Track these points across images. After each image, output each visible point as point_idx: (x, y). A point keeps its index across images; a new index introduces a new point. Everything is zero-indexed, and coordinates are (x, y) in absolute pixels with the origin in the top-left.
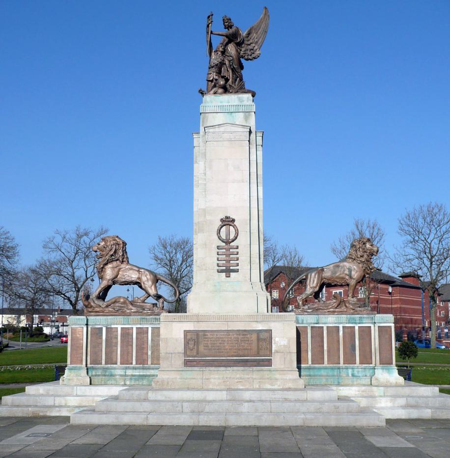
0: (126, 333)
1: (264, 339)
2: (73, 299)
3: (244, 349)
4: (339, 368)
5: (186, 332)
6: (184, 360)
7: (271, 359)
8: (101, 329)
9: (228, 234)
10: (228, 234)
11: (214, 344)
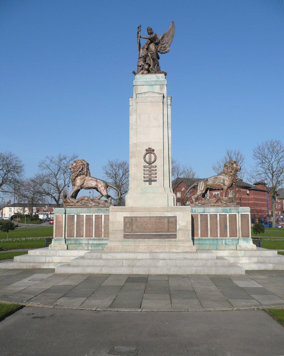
0: (89, 218)
1: (172, 222)
2: (57, 198)
3: (160, 228)
4: (217, 240)
5: (125, 218)
6: (124, 234)
7: (176, 234)
8: (74, 216)
9: (150, 158)
10: (150, 158)
11: (142, 225)
